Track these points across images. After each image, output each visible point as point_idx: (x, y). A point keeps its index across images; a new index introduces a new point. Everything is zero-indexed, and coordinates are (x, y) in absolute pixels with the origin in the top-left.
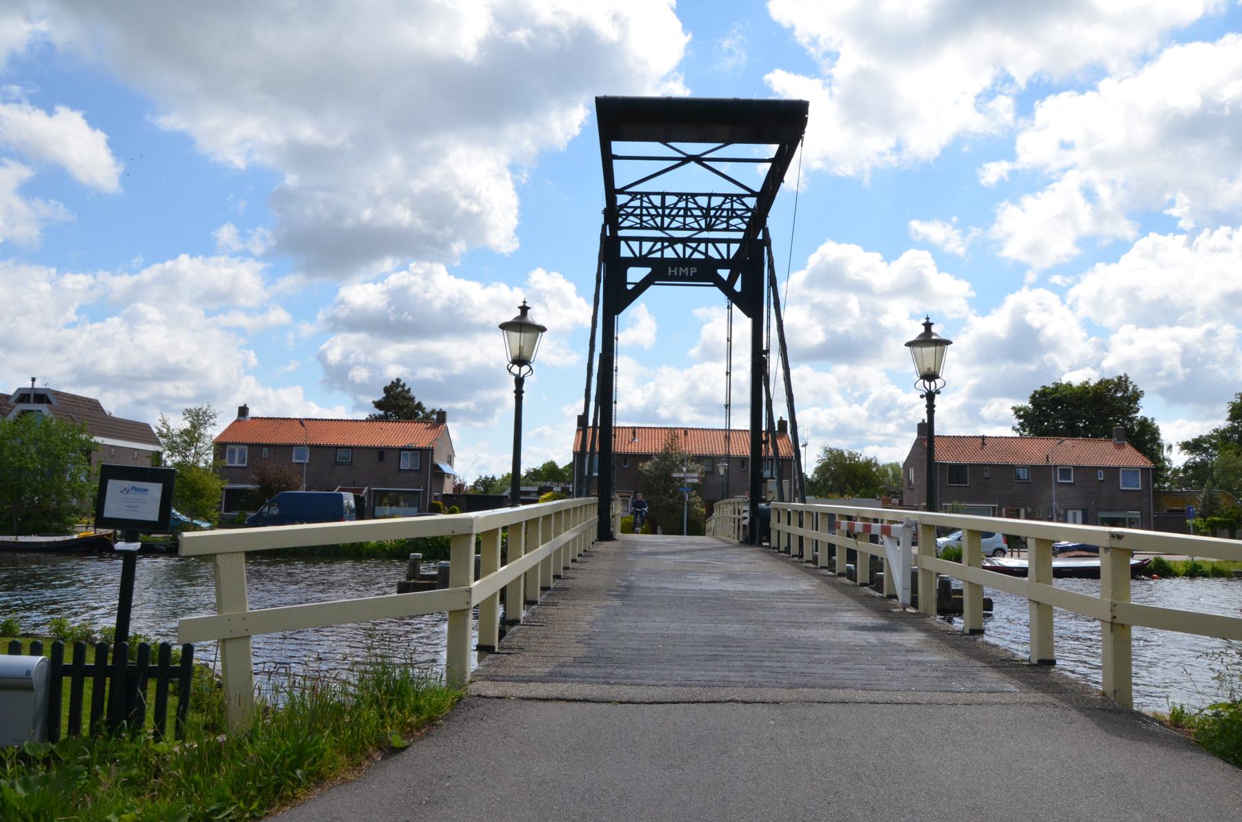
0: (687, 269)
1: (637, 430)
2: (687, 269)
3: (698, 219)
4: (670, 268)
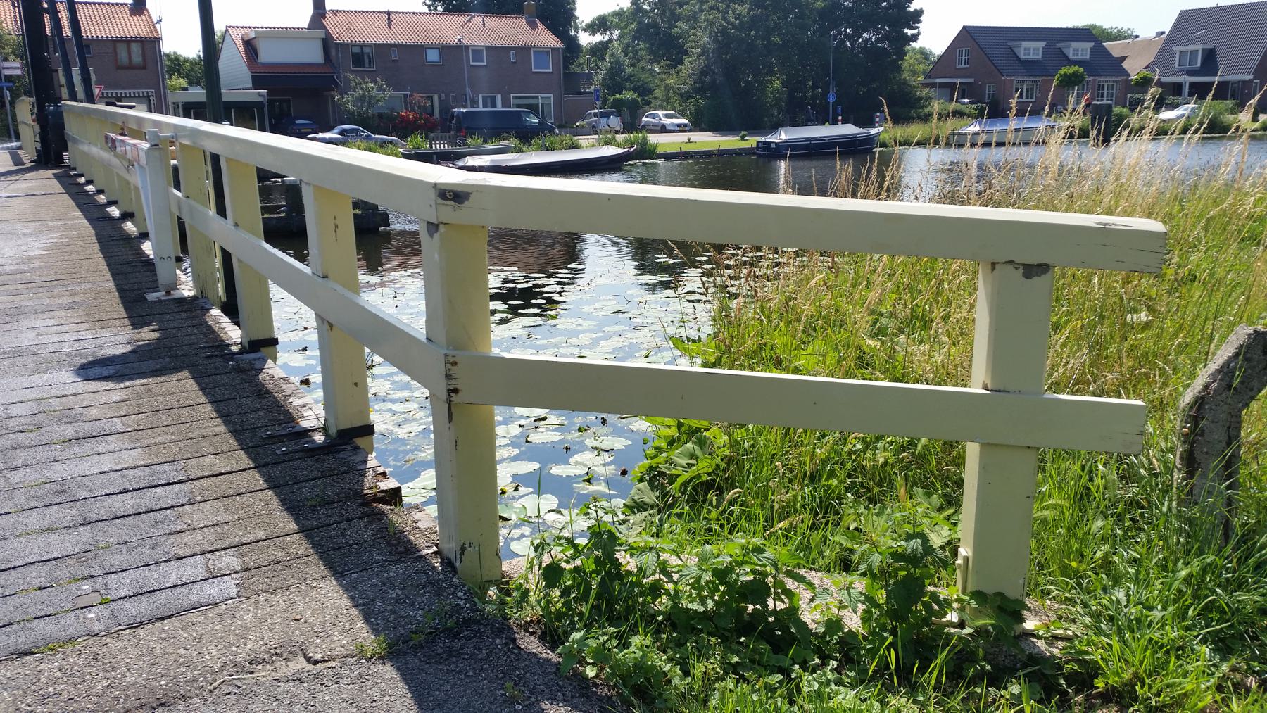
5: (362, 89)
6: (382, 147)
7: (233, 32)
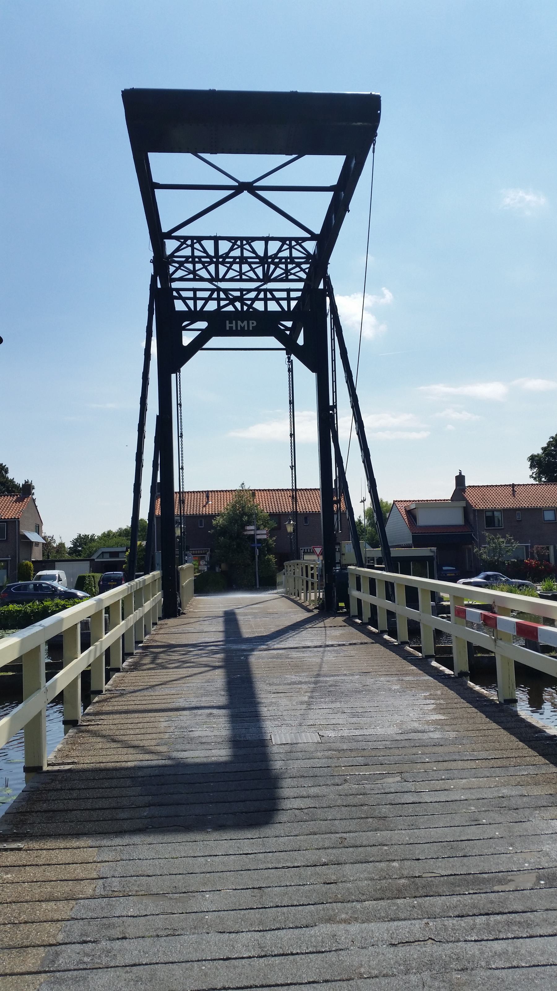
0: (245, 322)
1: (210, 494)
2: (245, 322)
3: (254, 266)
4: (227, 322)
5: (494, 543)
6: (519, 588)
7: (398, 505)
